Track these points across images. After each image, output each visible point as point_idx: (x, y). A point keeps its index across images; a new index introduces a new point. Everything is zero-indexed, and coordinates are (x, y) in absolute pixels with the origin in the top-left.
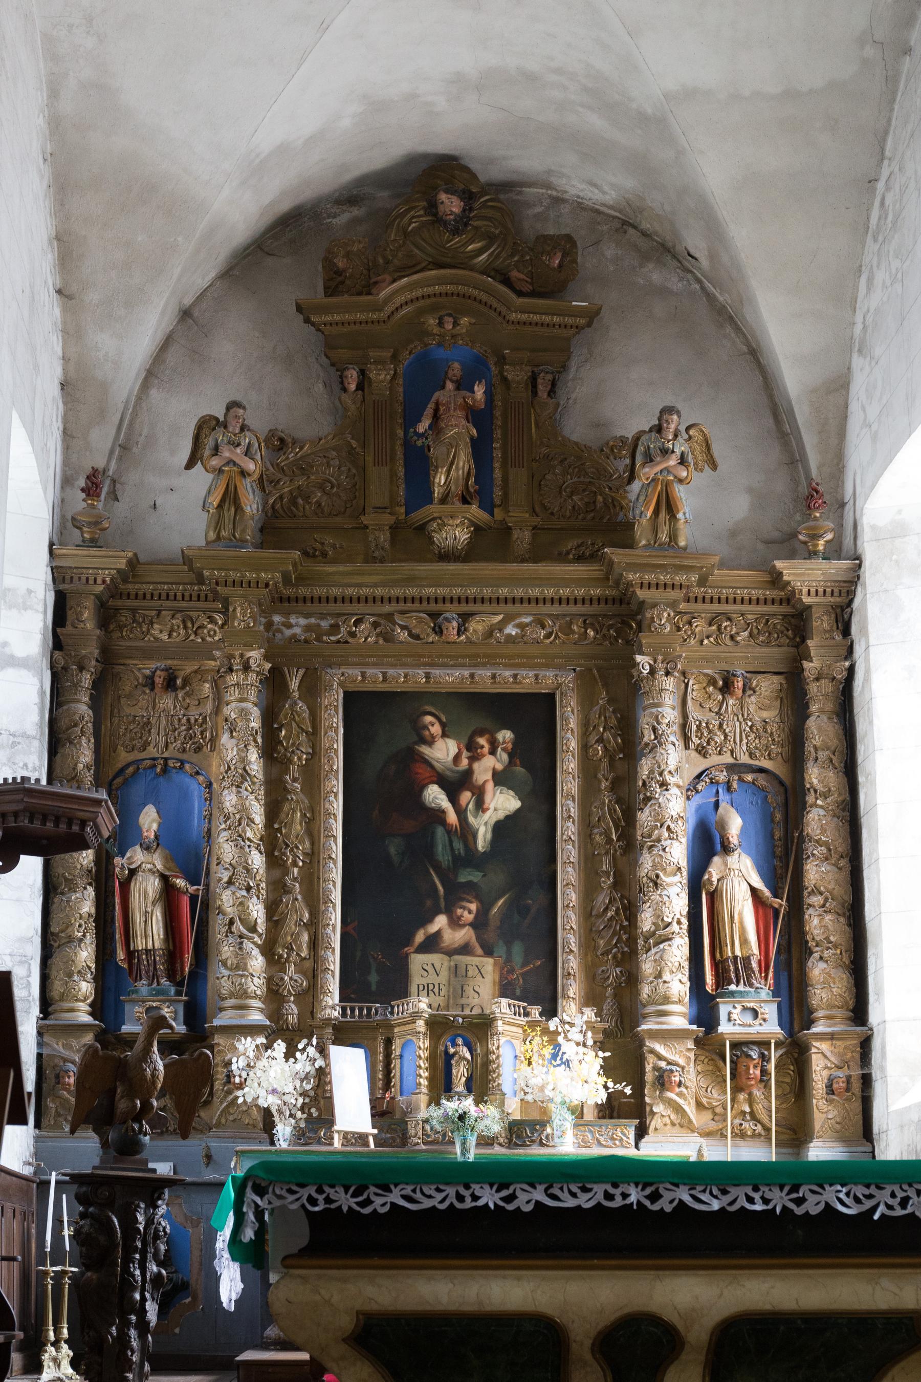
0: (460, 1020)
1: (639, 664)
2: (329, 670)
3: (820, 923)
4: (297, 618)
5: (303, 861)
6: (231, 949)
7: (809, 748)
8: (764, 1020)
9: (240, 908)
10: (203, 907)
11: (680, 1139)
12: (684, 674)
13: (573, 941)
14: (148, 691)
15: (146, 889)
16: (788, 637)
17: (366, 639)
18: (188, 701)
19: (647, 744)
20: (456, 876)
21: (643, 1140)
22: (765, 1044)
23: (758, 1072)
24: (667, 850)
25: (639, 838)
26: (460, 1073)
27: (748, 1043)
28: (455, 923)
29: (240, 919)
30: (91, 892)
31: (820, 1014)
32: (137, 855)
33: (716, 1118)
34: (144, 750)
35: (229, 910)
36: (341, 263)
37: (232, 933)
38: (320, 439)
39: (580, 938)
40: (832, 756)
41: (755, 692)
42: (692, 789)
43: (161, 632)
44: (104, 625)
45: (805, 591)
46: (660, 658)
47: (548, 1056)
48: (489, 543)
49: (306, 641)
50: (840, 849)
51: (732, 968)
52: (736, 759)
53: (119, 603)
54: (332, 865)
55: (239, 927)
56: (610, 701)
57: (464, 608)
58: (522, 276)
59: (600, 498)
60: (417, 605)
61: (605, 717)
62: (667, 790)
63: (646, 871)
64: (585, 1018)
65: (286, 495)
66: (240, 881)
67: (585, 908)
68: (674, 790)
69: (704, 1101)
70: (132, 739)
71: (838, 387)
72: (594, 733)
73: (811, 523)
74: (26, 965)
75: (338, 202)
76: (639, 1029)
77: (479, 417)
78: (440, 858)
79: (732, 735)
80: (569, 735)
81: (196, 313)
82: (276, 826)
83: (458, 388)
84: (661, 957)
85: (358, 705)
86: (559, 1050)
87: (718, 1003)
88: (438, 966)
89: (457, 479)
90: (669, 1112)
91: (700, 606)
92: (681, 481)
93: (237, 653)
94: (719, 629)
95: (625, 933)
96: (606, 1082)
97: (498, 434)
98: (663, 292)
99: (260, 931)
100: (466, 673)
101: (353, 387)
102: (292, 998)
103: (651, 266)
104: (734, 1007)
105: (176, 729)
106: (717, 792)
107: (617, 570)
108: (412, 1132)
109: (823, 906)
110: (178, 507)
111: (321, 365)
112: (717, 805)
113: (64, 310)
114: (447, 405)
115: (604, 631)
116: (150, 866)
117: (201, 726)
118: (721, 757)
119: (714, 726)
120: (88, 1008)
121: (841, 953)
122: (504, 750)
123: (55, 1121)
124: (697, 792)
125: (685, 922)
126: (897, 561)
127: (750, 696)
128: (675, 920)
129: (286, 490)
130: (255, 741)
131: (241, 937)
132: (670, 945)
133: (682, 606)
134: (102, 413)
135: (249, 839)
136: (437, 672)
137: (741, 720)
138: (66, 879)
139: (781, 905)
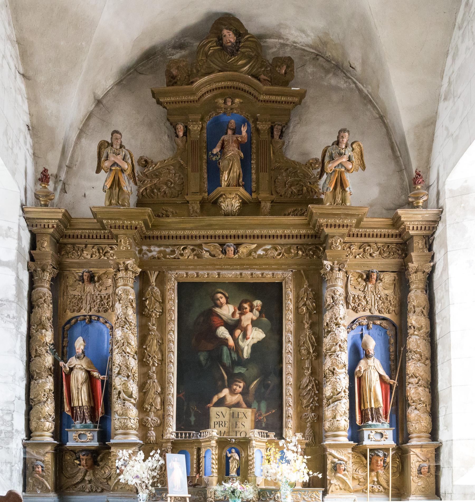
0: (234, 440)
1: (325, 265)
2: (170, 272)
3: (416, 391)
4: (154, 247)
5: (158, 364)
6: (119, 406)
7: (410, 306)
8: (386, 438)
9: (123, 386)
10: (108, 386)
11: (344, 496)
12: (346, 272)
13: (291, 401)
14: (81, 283)
15: (79, 377)
16: (398, 254)
17: (188, 257)
18: (101, 288)
19: (329, 305)
20: (233, 370)
21: (326, 497)
22: (387, 450)
23: (382, 463)
24: (339, 356)
25: (325, 351)
26: (233, 466)
27: (377, 449)
28: (233, 392)
29: (123, 391)
30: (51, 379)
31: (414, 435)
32: (73, 361)
33: (360, 484)
34: (80, 311)
35: (119, 387)
36: (174, 72)
37: (120, 398)
38: (165, 161)
39: (294, 399)
40: (423, 310)
41: (381, 281)
42: (350, 328)
43: (87, 255)
44: (58, 253)
45: (411, 228)
46: (336, 262)
47: (278, 458)
48: (249, 208)
49: (159, 258)
50: (426, 356)
51: (370, 413)
52: (372, 313)
53: (65, 241)
54: (172, 365)
55: (123, 395)
56: (310, 286)
57: (237, 241)
58: (266, 78)
59: (305, 188)
60: (213, 239)
61: (307, 294)
62: (339, 327)
63: (328, 366)
64: (297, 438)
65: (148, 188)
66: (124, 372)
67: (296, 385)
68: (342, 327)
69: (355, 476)
70: (73, 306)
71: (429, 125)
72: (302, 301)
73: (416, 192)
74: (11, 415)
75: (174, 47)
76: (324, 443)
77: (245, 147)
78: (225, 362)
79: (370, 302)
80: (289, 302)
81: (104, 102)
82: (144, 347)
83: (234, 134)
84: (336, 409)
85: (185, 289)
86: (284, 454)
87: (363, 430)
88: (224, 413)
89: (233, 178)
90: (339, 483)
91: (355, 239)
92: (348, 171)
93: (121, 262)
94: (364, 250)
95: (317, 397)
96: (308, 472)
97: (254, 156)
98: (336, 89)
99: (135, 397)
100: (238, 272)
101: (181, 134)
102: (153, 429)
103: (331, 75)
104: (371, 432)
105: (95, 301)
106: (362, 329)
107: (315, 218)
108: (209, 495)
109: (417, 383)
110: (90, 192)
111: (167, 127)
112: (362, 336)
113: (27, 86)
114: (228, 141)
115: (307, 252)
116: (79, 366)
117: (107, 299)
118: (364, 312)
119: (361, 297)
120: (51, 434)
121: (426, 406)
122: (257, 310)
123: (33, 489)
124: (352, 329)
125: (347, 391)
126: (464, 207)
127: (379, 283)
128: (343, 390)
129: (149, 185)
130: (132, 305)
131: (124, 400)
132: (340, 403)
133: (347, 239)
134: (53, 145)
135: (128, 353)
136: (224, 272)
137: (375, 294)
138: (37, 373)
139: (394, 383)
